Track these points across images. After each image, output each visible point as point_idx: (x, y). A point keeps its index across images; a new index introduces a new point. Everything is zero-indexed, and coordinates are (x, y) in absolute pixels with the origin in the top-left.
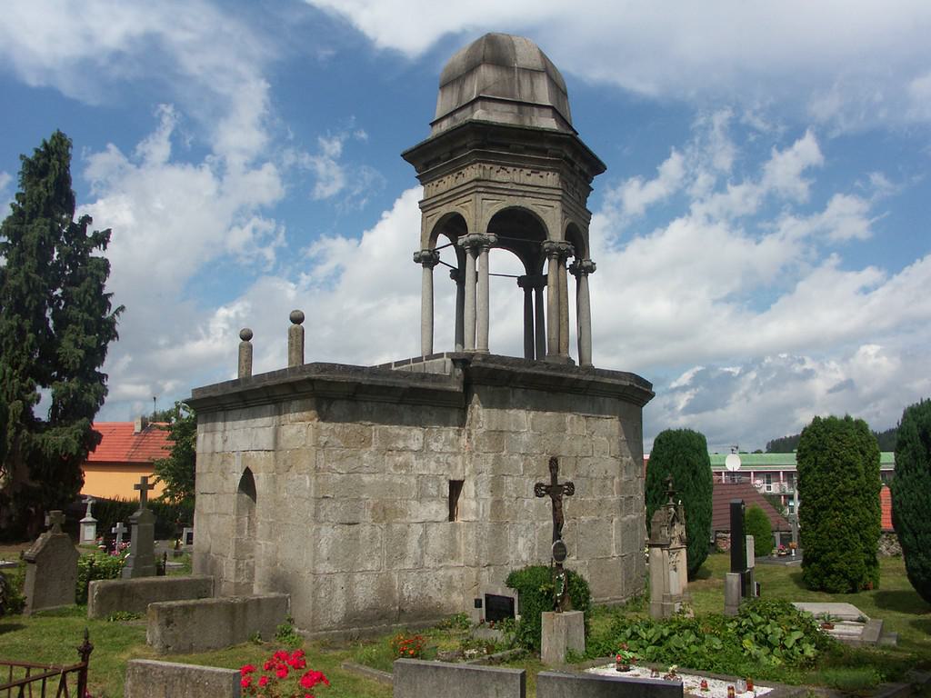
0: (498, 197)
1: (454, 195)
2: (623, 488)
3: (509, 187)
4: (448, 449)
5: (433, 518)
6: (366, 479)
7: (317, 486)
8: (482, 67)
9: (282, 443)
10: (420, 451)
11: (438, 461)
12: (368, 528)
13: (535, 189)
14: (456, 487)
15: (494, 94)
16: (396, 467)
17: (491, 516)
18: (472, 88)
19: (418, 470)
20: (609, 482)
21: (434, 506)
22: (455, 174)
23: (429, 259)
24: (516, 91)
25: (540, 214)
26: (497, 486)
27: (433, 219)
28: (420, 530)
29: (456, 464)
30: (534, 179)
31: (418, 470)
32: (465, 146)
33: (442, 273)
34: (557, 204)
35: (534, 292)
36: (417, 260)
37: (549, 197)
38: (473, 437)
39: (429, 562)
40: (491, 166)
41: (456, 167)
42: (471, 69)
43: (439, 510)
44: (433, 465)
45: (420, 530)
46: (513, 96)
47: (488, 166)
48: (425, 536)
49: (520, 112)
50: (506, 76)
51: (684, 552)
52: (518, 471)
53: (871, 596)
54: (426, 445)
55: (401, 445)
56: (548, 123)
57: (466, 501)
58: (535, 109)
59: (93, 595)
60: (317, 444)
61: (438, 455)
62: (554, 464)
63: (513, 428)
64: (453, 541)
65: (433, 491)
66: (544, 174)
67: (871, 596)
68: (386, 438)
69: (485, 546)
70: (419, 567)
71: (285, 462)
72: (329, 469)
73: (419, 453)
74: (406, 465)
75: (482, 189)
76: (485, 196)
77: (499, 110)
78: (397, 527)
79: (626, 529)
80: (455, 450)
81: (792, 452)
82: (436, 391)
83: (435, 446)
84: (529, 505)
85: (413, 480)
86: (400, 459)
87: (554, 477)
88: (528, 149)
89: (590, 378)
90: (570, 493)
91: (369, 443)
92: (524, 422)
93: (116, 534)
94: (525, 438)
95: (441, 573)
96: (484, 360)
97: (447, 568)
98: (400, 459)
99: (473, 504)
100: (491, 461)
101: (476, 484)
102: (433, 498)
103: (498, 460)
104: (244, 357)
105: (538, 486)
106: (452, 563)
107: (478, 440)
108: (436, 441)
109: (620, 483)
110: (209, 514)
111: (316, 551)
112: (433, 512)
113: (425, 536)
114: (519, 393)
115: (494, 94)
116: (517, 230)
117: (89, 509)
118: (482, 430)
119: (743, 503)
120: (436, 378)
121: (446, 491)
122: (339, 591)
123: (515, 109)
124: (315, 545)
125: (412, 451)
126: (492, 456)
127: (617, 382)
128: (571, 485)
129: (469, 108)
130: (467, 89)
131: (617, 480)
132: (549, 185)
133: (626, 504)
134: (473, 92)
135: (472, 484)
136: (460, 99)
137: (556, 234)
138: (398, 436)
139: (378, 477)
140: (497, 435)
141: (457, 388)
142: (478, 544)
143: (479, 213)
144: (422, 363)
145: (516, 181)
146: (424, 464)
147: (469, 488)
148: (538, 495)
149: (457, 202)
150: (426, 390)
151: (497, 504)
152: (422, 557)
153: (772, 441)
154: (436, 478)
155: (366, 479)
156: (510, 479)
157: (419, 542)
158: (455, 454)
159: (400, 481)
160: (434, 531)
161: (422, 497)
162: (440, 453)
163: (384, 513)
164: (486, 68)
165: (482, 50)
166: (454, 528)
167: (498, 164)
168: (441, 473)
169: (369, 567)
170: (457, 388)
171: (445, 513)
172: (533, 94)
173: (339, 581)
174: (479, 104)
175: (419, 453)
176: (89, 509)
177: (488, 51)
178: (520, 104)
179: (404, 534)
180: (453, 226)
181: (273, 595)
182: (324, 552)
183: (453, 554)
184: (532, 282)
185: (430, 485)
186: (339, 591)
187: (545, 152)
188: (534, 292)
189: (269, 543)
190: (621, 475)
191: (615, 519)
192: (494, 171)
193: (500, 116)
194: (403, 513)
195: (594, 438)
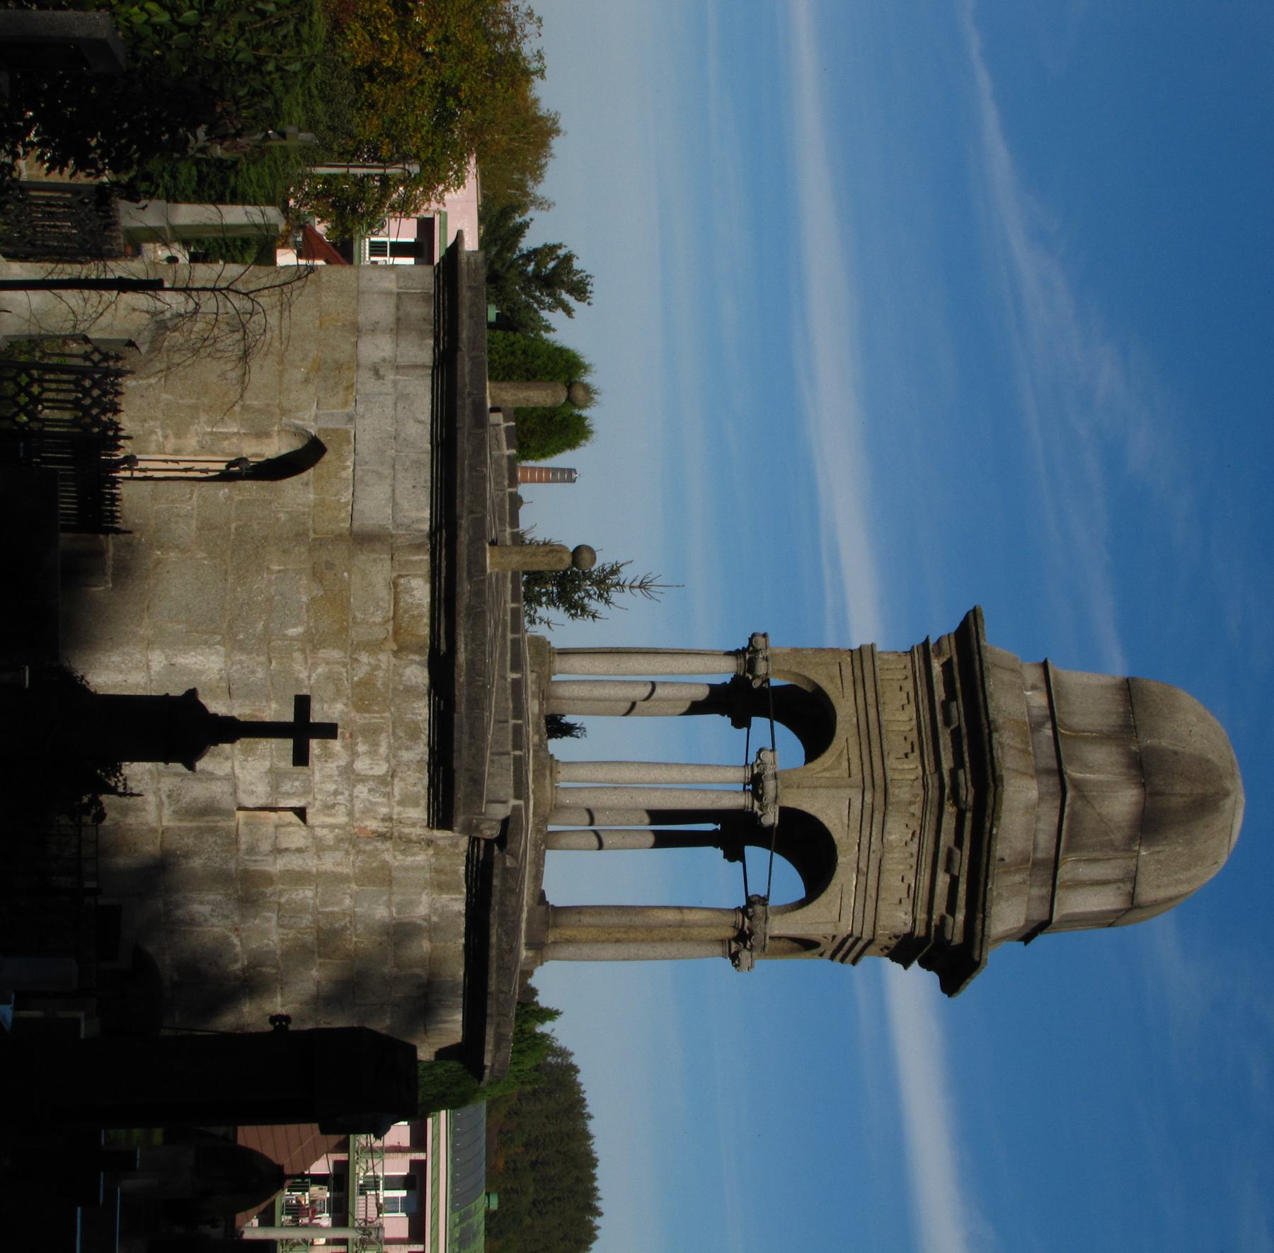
3: (873, 847)
4: (359, 806)
5: (241, 787)
9: (363, 558)
10: (353, 771)
11: (336, 793)
15: (1074, 815)
18: (1099, 767)
19: (322, 769)
22: (913, 736)
24: (1085, 855)
27: (832, 679)
29: (334, 815)
31: (322, 769)
34: (845, 928)
35: (709, 827)
37: (859, 915)
38: (379, 844)
40: (918, 813)
42: (1144, 767)
44: (331, 787)
46: (1069, 849)
47: (916, 809)
49: (1037, 864)
50: (1118, 838)
53: (460, 235)
54: (362, 779)
55: (362, 748)
56: (1008, 913)
58: (1045, 891)
61: (347, 793)
67: (460, 235)
75: (868, 799)
77: (1041, 825)
80: (357, 815)
81: (785, 813)
83: (362, 791)
84: (268, 920)
91: (360, 709)
97: (160, 805)
100: (339, 869)
103: (345, 879)
107: (373, 854)
108: (370, 790)
112: (253, 787)
125: (353, 762)
134: (1090, 769)
136: (1080, 737)
138: (375, 745)
144: (510, 748)
145: (888, 856)
146: (331, 776)
149: (853, 741)
153: (574, 1069)
154: (307, 791)
158: (350, 814)
162: (351, 795)
164: (1133, 799)
167: (922, 827)
168: (319, 797)
172: (1078, 884)
177: (1176, 802)
185: (297, 784)
186: (120, 678)
189: (194, 524)
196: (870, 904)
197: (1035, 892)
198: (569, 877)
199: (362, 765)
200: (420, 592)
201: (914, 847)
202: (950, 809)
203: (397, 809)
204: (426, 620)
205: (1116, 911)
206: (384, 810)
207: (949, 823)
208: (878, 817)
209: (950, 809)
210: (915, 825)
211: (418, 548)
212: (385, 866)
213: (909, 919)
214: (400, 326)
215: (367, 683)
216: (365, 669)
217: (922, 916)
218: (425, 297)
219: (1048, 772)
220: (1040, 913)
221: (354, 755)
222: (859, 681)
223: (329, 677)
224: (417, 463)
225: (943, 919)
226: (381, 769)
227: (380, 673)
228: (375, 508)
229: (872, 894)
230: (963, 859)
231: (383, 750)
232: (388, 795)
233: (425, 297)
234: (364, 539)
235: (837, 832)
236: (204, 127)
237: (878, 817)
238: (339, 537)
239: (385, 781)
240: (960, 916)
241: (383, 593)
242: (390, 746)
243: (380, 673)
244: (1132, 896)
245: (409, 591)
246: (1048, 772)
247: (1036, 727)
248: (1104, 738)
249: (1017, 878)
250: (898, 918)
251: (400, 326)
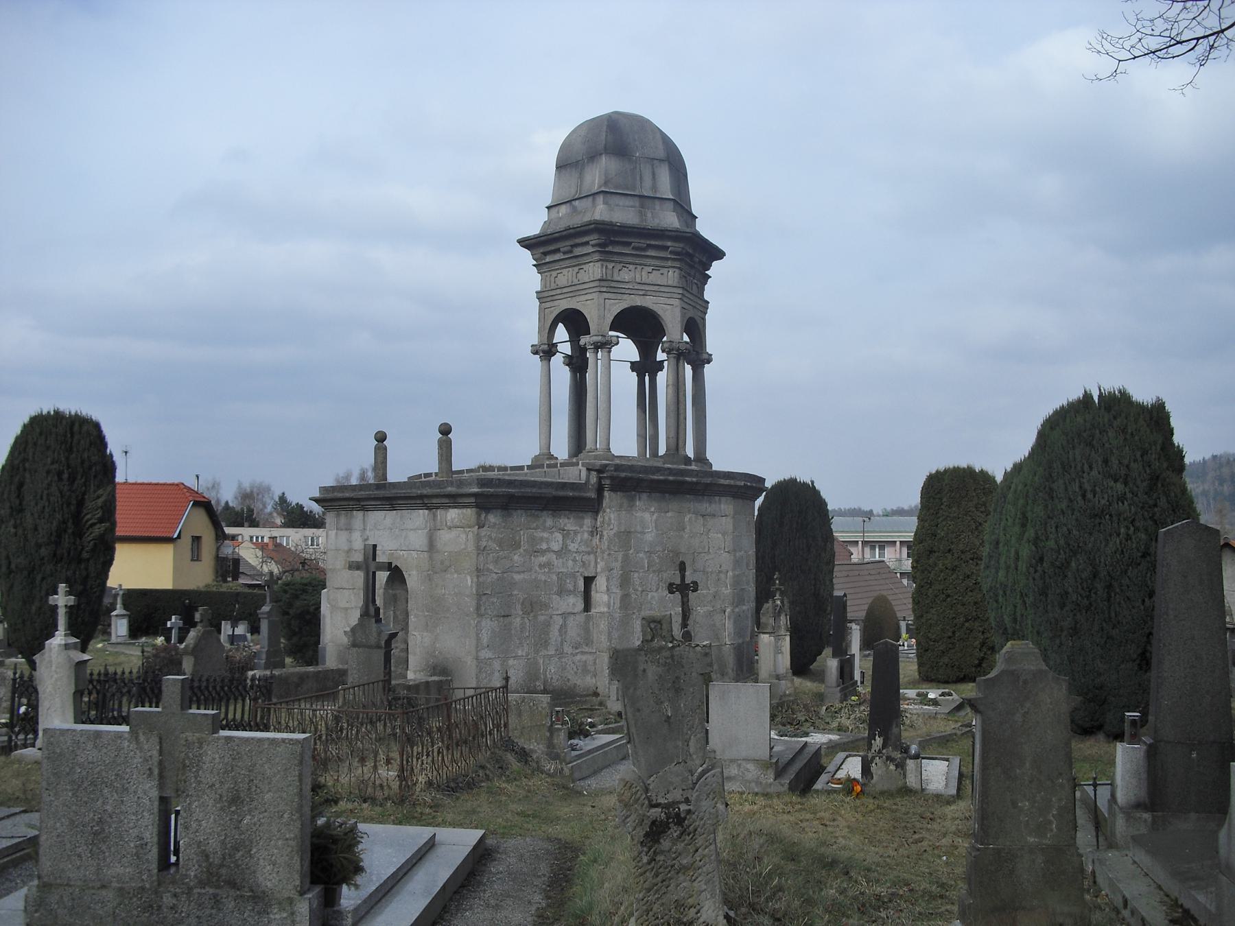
0: (619, 296)
1: (575, 289)
2: (737, 582)
4: (583, 548)
5: (570, 610)
6: (517, 577)
7: (479, 585)
8: (603, 157)
9: (439, 545)
11: (574, 560)
12: (518, 619)
13: (656, 288)
14: (589, 581)
16: (540, 566)
17: (620, 608)
20: (722, 576)
21: (571, 600)
22: (576, 269)
23: (547, 351)
25: (660, 312)
26: (625, 581)
28: (560, 621)
30: (655, 277)
32: (587, 243)
33: (557, 360)
34: (677, 302)
35: (647, 378)
36: (536, 353)
39: (568, 649)
41: (577, 261)
43: (577, 603)
44: (570, 562)
45: (560, 621)
47: (610, 266)
48: (563, 628)
49: (642, 206)
51: (788, 638)
52: (643, 567)
54: (565, 546)
55: (544, 546)
56: (670, 220)
57: (601, 596)
58: (657, 202)
59: (1161, 537)
60: (478, 548)
62: (682, 567)
63: (639, 528)
64: (587, 630)
65: (570, 587)
66: (664, 271)
68: (533, 540)
69: (615, 635)
70: (560, 653)
71: (442, 563)
72: (488, 570)
73: (558, 554)
74: (548, 564)
76: (607, 295)
78: (541, 618)
79: (738, 619)
82: (573, 498)
83: (573, 547)
84: (653, 597)
85: (555, 577)
86: (543, 559)
87: (683, 577)
88: (650, 246)
89: (708, 480)
90: (671, 585)
92: (648, 518)
93: (171, 629)
94: (649, 537)
95: (578, 657)
96: (616, 470)
97: (583, 653)
98: (543, 559)
99: (605, 598)
100: (620, 559)
101: (608, 580)
102: (570, 592)
103: (626, 559)
104: (380, 459)
105: (671, 585)
106: (587, 649)
107: (610, 541)
109: (735, 576)
110: (346, 609)
111: (478, 639)
113: (563, 628)
114: (644, 496)
115: (616, 187)
116: (640, 325)
117: (119, 600)
118: (612, 533)
119: (845, 595)
120: (573, 486)
121: (581, 583)
122: (497, 674)
123: (637, 202)
124: (477, 635)
126: (620, 556)
127: (732, 482)
128: (695, 583)
129: (590, 199)
130: (588, 178)
131: (730, 573)
132: (670, 283)
133: (739, 600)
134: (593, 182)
135: (604, 579)
137: (675, 333)
138: (542, 539)
139: (526, 576)
140: (625, 537)
141: (593, 495)
142: (609, 633)
143: (599, 311)
147: (601, 583)
148: (671, 592)
149: (578, 299)
150: (566, 498)
151: (625, 597)
152: (562, 644)
154: (573, 576)
155: (517, 577)
156: (636, 575)
157: (560, 631)
158: (589, 553)
159: (543, 578)
160: (571, 622)
161: (562, 592)
163: (532, 606)
165: (603, 137)
166: (588, 619)
169: (520, 653)
170: (593, 495)
171: (581, 606)
172: (654, 188)
173: (497, 665)
174: (600, 199)
175: (558, 554)
176: (119, 600)
178: (641, 197)
179: (548, 624)
180: (576, 322)
181: (435, 678)
182: (485, 641)
183: (588, 641)
184: (645, 368)
186: (497, 674)
187: (666, 248)
188: (647, 378)
190: (733, 570)
191: (728, 610)
192: (616, 271)
193: (624, 214)
194: (546, 606)
195: (711, 535)
196: (662, 289)
197: (657, 207)
198: (623, 439)
199: (556, 547)
200: (453, 514)
201: (631, 267)
202: (610, 249)
203: (585, 528)
204: (464, 510)
205: (670, 169)
206: (586, 535)
207: (617, 249)
208: (613, 284)
209: (610, 249)
210: (619, 266)
211: (435, 516)
212: (618, 534)
213: (671, 271)
214: (349, 529)
215: (500, 543)
216: (490, 543)
217: (669, 263)
218: (338, 516)
219: (594, 200)
220: (670, 205)
221: (549, 550)
222: (552, 298)
223: (496, 562)
224: (402, 517)
225: (671, 253)
226: (559, 536)
227: (493, 535)
228: (418, 539)
229: (657, 289)
230: (636, 242)
231: (545, 535)
232: (576, 533)
233: (338, 516)
234: (431, 546)
235: (624, 305)
236: (828, 651)
237: (613, 284)
238: (431, 558)
239: (566, 534)
240: (669, 244)
241: (454, 533)
242: (544, 531)
243: (493, 535)
244: (661, 160)
245: (452, 520)
246: (594, 200)
247: (575, 209)
248: (581, 177)
249: (649, 215)
250: (671, 276)
251: (349, 529)
